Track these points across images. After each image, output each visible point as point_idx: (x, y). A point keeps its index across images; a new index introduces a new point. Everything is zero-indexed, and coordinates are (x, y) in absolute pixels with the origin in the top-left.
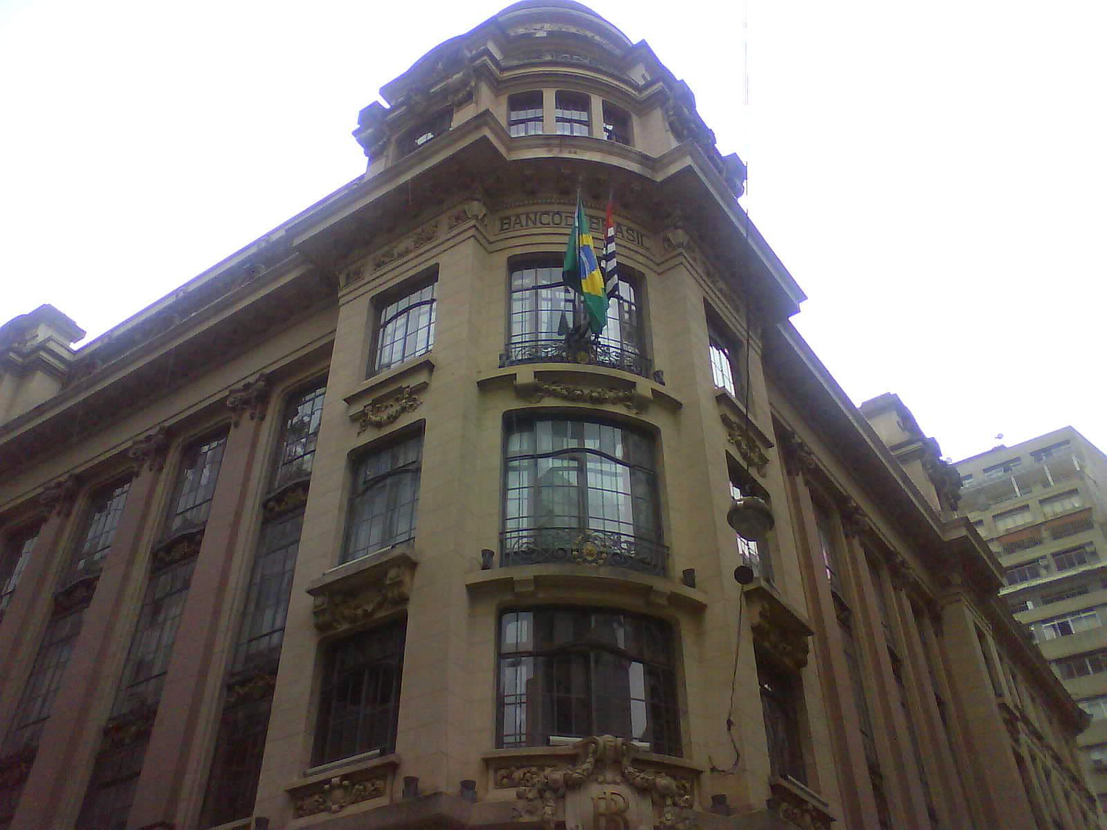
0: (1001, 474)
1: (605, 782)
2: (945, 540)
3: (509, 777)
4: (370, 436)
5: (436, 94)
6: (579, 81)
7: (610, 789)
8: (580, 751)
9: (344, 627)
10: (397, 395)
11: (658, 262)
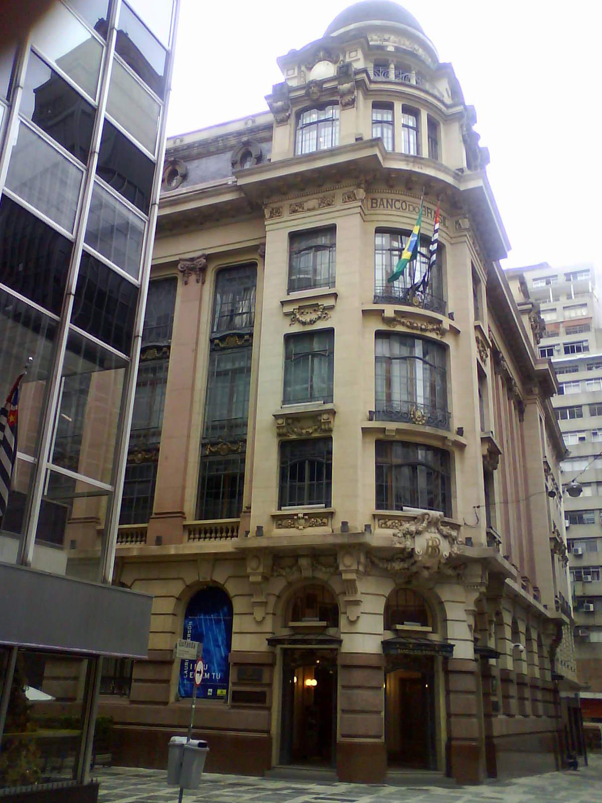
0: (544, 284)
1: (431, 532)
2: (384, 166)
3: (385, 523)
4: (296, 329)
5: (327, 89)
6: (416, 99)
7: (433, 535)
9: (294, 437)
10: (315, 307)
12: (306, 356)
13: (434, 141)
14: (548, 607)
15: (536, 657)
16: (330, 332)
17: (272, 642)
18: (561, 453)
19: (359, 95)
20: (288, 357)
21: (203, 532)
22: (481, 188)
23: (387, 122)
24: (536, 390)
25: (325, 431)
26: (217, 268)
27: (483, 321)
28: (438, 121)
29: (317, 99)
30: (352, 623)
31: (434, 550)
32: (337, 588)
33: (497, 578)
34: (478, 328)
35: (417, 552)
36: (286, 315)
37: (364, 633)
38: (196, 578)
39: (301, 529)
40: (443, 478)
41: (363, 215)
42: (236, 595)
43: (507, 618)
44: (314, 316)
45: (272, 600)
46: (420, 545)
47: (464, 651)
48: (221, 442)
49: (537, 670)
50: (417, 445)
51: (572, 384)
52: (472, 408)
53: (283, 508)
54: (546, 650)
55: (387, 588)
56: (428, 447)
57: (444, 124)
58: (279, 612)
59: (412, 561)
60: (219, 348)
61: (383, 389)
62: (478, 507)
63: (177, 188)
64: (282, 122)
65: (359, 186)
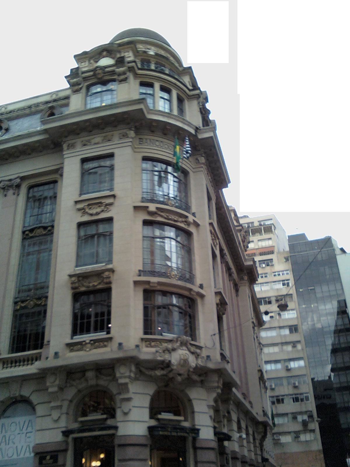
3: (150, 344)
4: (86, 218)
5: (108, 72)
8: (175, 339)
11: (194, 167)
12: (92, 236)
13: (181, 110)
14: (258, 414)
15: (252, 446)
16: (110, 220)
17: (66, 433)
18: (260, 323)
19: (131, 76)
20: (79, 237)
21: (14, 362)
22: (211, 137)
23: (150, 94)
24: (246, 278)
25: (107, 283)
26: (28, 186)
27: (213, 220)
28: (183, 98)
29: (101, 78)
30: (126, 414)
31: (185, 362)
32: (114, 391)
33: (228, 385)
34: (211, 224)
35: (173, 363)
36: (79, 210)
37: (135, 421)
38: (7, 395)
39: (87, 351)
40: (190, 316)
41: (134, 148)
42: (38, 404)
43: (234, 417)
44: (99, 210)
45: (66, 404)
46: (175, 358)
47: (207, 434)
48: (29, 299)
49: (253, 454)
50: (172, 293)
51: (265, 284)
52: (208, 277)
53: (75, 337)
54: (258, 442)
55: (151, 389)
56: (180, 296)
57: (188, 101)
58: (71, 412)
59: (169, 369)
60: (29, 237)
61: (148, 256)
62: (214, 335)
63: (2, 136)
64: (76, 92)
65: (130, 129)
